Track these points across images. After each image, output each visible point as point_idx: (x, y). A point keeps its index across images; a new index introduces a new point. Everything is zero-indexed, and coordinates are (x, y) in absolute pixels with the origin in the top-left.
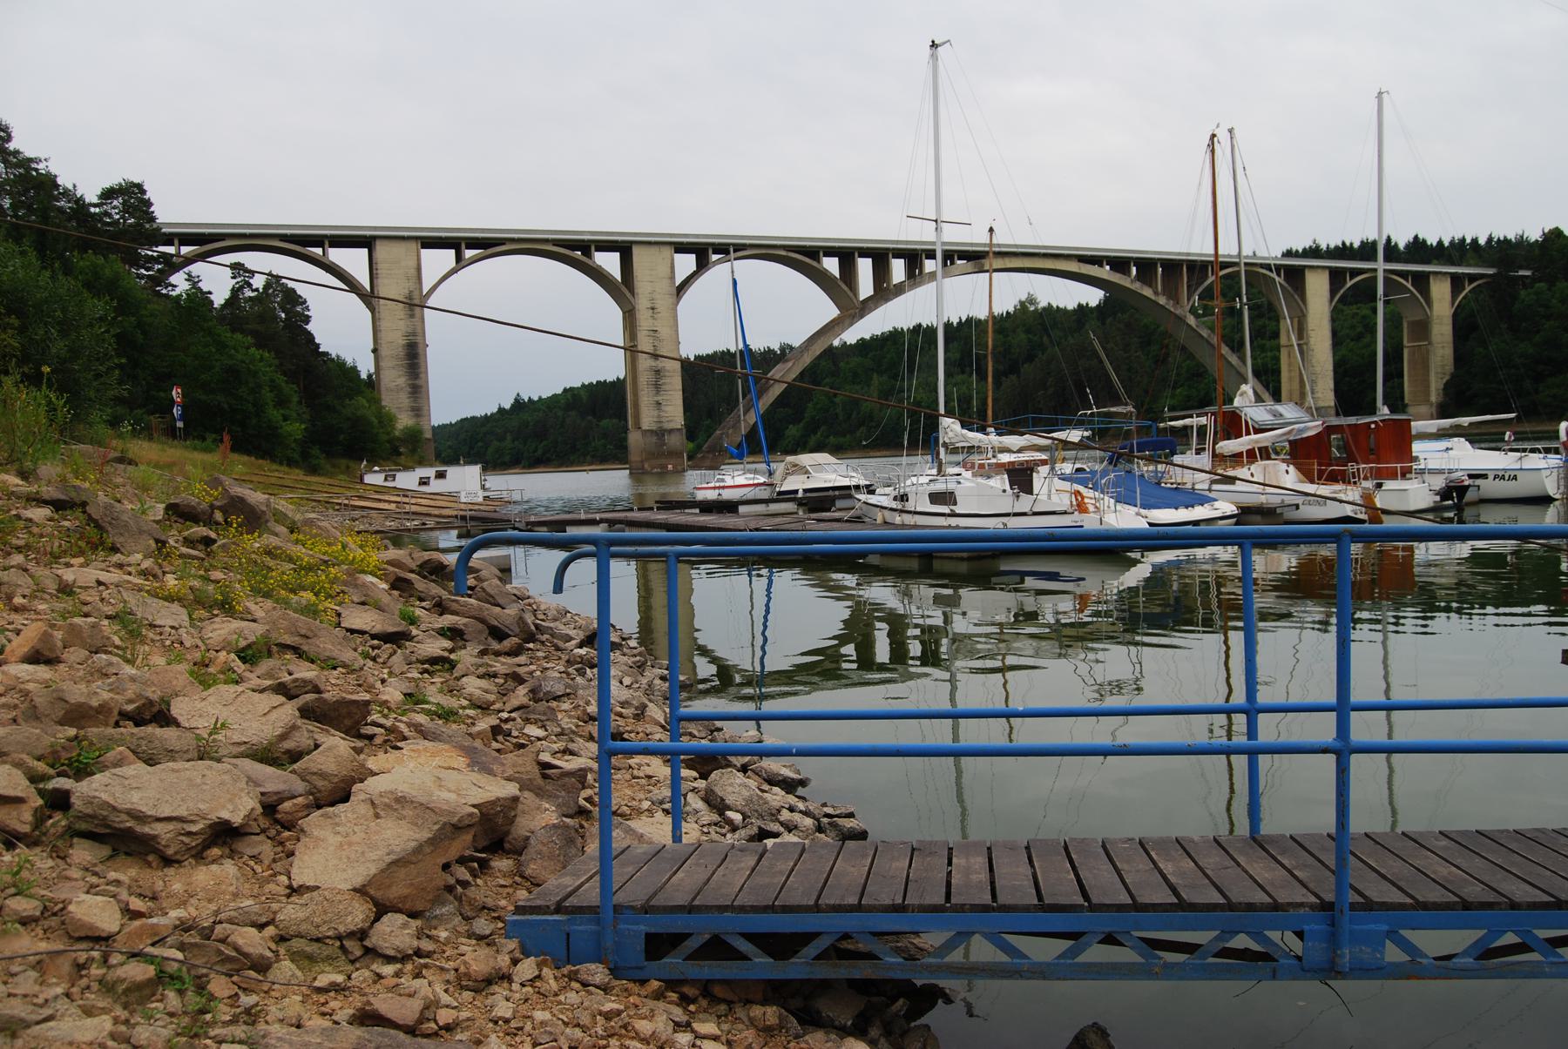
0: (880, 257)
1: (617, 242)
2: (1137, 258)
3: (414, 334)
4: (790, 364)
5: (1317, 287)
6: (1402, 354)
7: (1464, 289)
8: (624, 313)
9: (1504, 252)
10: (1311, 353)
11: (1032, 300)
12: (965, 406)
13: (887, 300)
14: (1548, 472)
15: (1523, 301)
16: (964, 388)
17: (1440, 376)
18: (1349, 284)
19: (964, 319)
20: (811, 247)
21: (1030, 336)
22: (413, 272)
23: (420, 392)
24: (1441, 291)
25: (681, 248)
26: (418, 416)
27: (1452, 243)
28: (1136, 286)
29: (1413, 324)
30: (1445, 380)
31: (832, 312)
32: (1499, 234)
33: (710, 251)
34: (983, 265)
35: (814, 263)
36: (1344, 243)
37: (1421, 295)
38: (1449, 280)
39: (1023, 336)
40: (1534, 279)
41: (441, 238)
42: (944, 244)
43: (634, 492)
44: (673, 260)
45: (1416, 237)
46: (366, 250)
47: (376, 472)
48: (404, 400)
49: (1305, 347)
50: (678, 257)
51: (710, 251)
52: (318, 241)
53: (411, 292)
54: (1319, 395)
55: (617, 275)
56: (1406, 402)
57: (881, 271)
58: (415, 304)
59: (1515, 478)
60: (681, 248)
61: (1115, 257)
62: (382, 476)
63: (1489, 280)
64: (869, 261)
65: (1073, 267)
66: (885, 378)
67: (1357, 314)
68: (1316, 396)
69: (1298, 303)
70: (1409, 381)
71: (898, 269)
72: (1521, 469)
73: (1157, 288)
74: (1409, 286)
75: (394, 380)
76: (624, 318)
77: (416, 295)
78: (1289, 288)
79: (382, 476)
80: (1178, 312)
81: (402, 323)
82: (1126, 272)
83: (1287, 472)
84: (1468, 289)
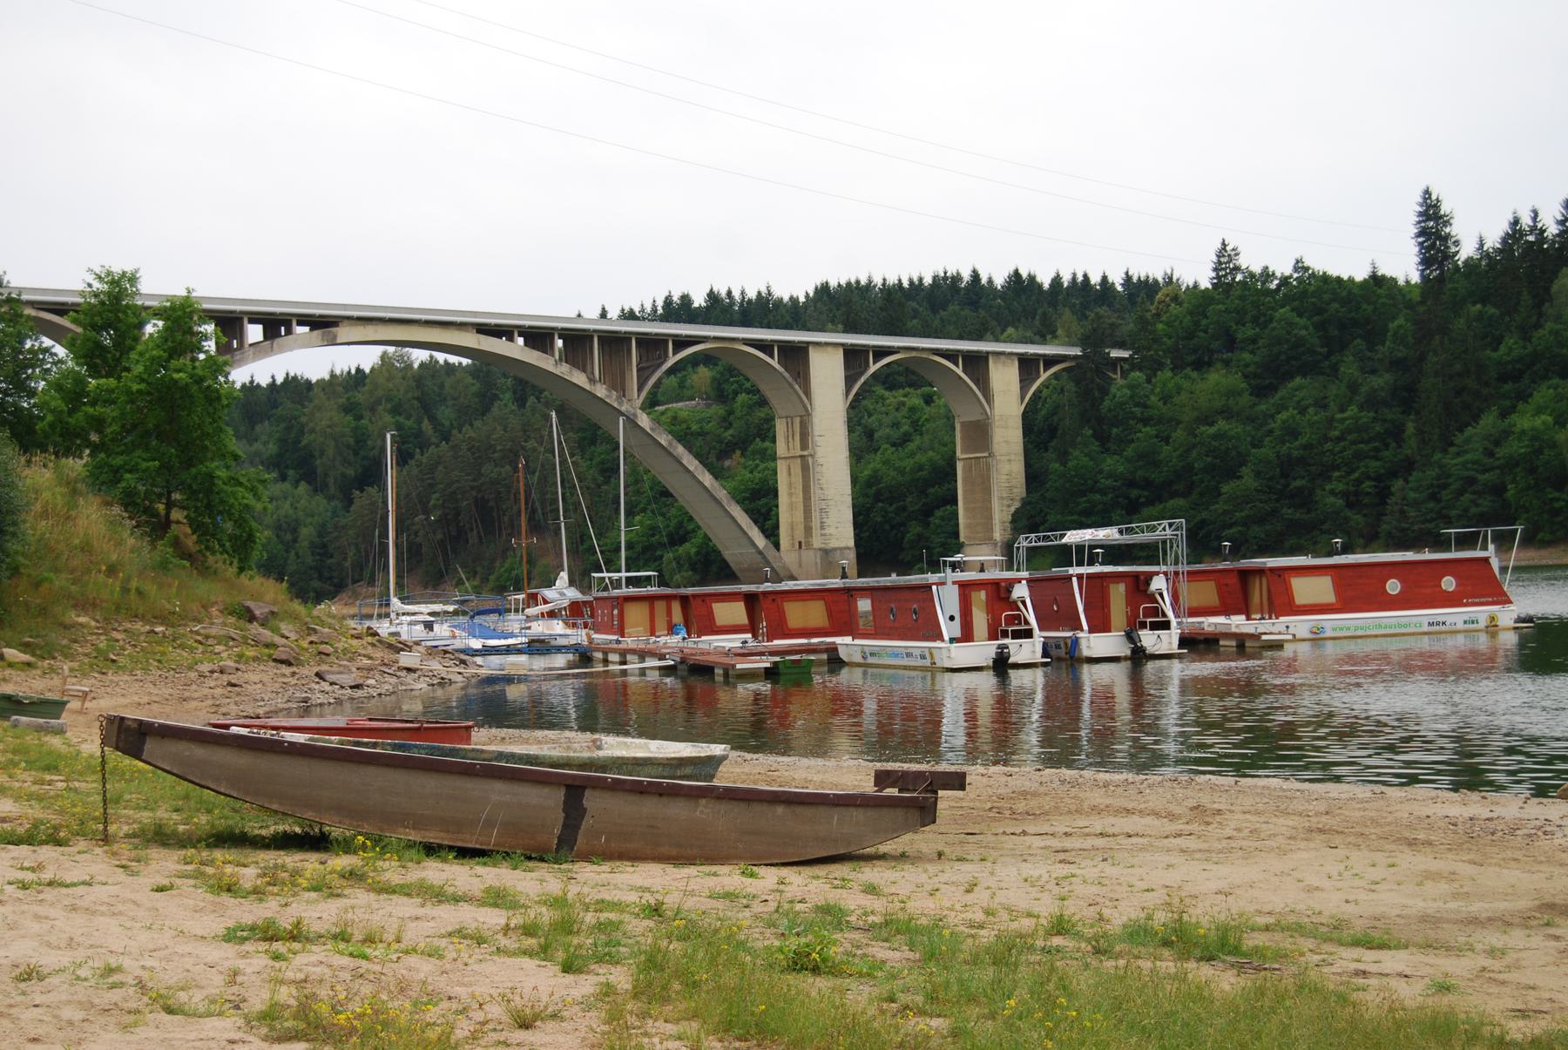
2: (563, 329)
6: (955, 470)
10: (818, 469)
12: (289, 537)
15: (1114, 397)
16: (287, 505)
17: (1005, 502)
18: (873, 368)
19: (280, 380)
21: (401, 419)
28: (563, 370)
29: (967, 426)
30: (1013, 509)
32: (1139, 271)
34: (335, 337)
37: (977, 383)
38: (1016, 363)
43: (700, 533)
45: (1017, 273)
49: (810, 460)
56: (962, 539)
63: (1073, 364)
67: (904, 404)
68: (826, 531)
70: (966, 509)
73: (593, 373)
74: (959, 371)
78: (786, 375)
84: (1044, 376)
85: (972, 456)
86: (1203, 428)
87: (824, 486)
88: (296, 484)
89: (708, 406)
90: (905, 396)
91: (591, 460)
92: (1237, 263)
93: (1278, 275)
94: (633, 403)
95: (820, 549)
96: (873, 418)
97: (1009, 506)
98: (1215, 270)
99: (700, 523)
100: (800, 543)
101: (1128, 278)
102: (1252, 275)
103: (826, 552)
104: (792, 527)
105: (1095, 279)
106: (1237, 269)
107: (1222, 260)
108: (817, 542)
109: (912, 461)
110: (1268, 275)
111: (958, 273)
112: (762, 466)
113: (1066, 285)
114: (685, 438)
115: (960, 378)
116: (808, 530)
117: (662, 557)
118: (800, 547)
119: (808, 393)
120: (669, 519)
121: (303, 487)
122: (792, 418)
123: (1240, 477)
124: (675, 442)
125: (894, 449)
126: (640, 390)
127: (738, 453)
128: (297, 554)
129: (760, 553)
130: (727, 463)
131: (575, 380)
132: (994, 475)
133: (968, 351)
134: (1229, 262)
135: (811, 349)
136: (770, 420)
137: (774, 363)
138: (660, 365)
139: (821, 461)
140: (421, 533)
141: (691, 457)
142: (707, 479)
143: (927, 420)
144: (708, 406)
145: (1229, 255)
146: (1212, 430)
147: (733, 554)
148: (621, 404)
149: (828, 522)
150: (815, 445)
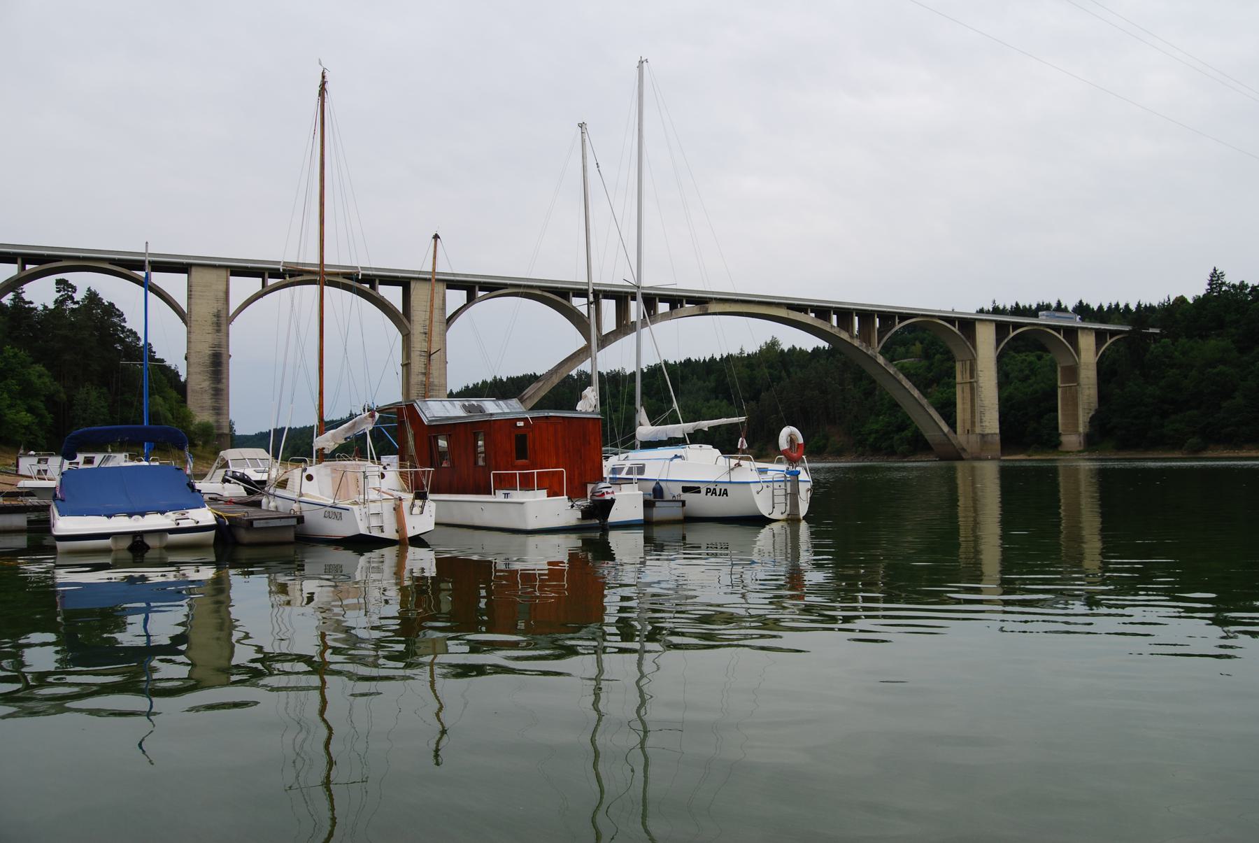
0: (622, 299)
1: (397, 277)
2: (836, 308)
3: (219, 346)
4: (541, 384)
5: (986, 338)
7: (1106, 342)
8: (403, 336)
9: (1144, 315)
11: (773, 344)
13: (626, 334)
14: (759, 487)
15: (1152, 352)
16: (716, 410)
17: (1087, 411)
18: (1012, 335)
19: (725, 356)
20: (562, 288)
22: (222, 295)
23: (222, 395)
24: (1087, 343)
25: (453, 285)
26: (218, 414)
27: (1110, 307)
29: (1064, 369)
30: (1090, 415)
31: (581, 342)
33: (477, 288)
35: (565, 302)
36: (1017, 304)
38: (1094, 334)
39: (766, 370)
40: (1160, 335)
41: (247, 268)
42: (595, 284)
44: (444, 294)
45: (1081, 302)
46: (261, 279)
47: (32, 455)
48: (207, 400)
49: (975, 384)
50: (450, 292)
51: (477, 288)
52: (139, 265)
53: (219, 311)
54: (987, 424)
55: (399, 305)
56: (1060, 431)
57: (622, 312)
58: (222, 321)
59: (726, 492)
60: (453, 285)
61: (817, 306)
62: (36, 459)
64: (613, 302)
65: (783, 313)
66: (654, 400)
67: (1025, 360)
69: (969, 348)
70: (1063, 415)
71: (635, 310)
72: (730, 482)
74: (1061, 338)
75: (198, 385)
76: (403, 340)
77: (223, 314)
78: (962, 337)
79: (36, 459)
80: (869, 353)
81: (210, 336)
82: (828, 319)
83: (310, 478)
84: (1109, 342)
85: (1067, 385)
86: (1210, 370)
87: (983, 399)
88: (721, 401)
89: (920, 361)
90: (1026, 356)
91: (859, 388)
92: (1224, 281)
93: (1250, 285)
94: (875, 350)
95: (980, 434)
96: (1009, 367)
97: (1088, 413)
98: (1209, 284)
99: (914, 420)
100: (968, 430)
101: (1139, 305)
102: (1234, 286)
103: (983, 436)
104: (964, 421)
105: (1122, 306)
106: (1223, 283)
107: (1214, 279)
108: (978, 430)
109: (1031, 388)
110: (1244, 285)
111: (1050, 304)
112: (948, 391)
113: (1105, 310)
114: (908, 376)
115: (1062, 341)
116: (973, 423)
117: (893, 437)
118: (968, 432)
119: (974, 346)
120: (897, 418)
121: (725, 402)
122: (965, 361)
123: (1234, 398)
124: (898, 372)
125: (1020, 383)
126: (879, 343)
127: (935, 385)
128: (720, 434)
129: (945, 435)
130: (929, 390)
131: (842, 336)
132: (1080, 396)
133: (1067, 327)
134: (1218, 280)
135: (977, 323)
136: (953, 368)
137: (956, 330)
138: (890, 330)
139: (981, 385)
140: (775, 424)
141: (907, 380)
142: (916, 393)
143: (1039, 368)
144: (920, 361)
145: (1218, 276)
146: (1215, 371)
147: (930, 435)
148: (868, 350)
149: (984, 419)
150: (978, 376)
